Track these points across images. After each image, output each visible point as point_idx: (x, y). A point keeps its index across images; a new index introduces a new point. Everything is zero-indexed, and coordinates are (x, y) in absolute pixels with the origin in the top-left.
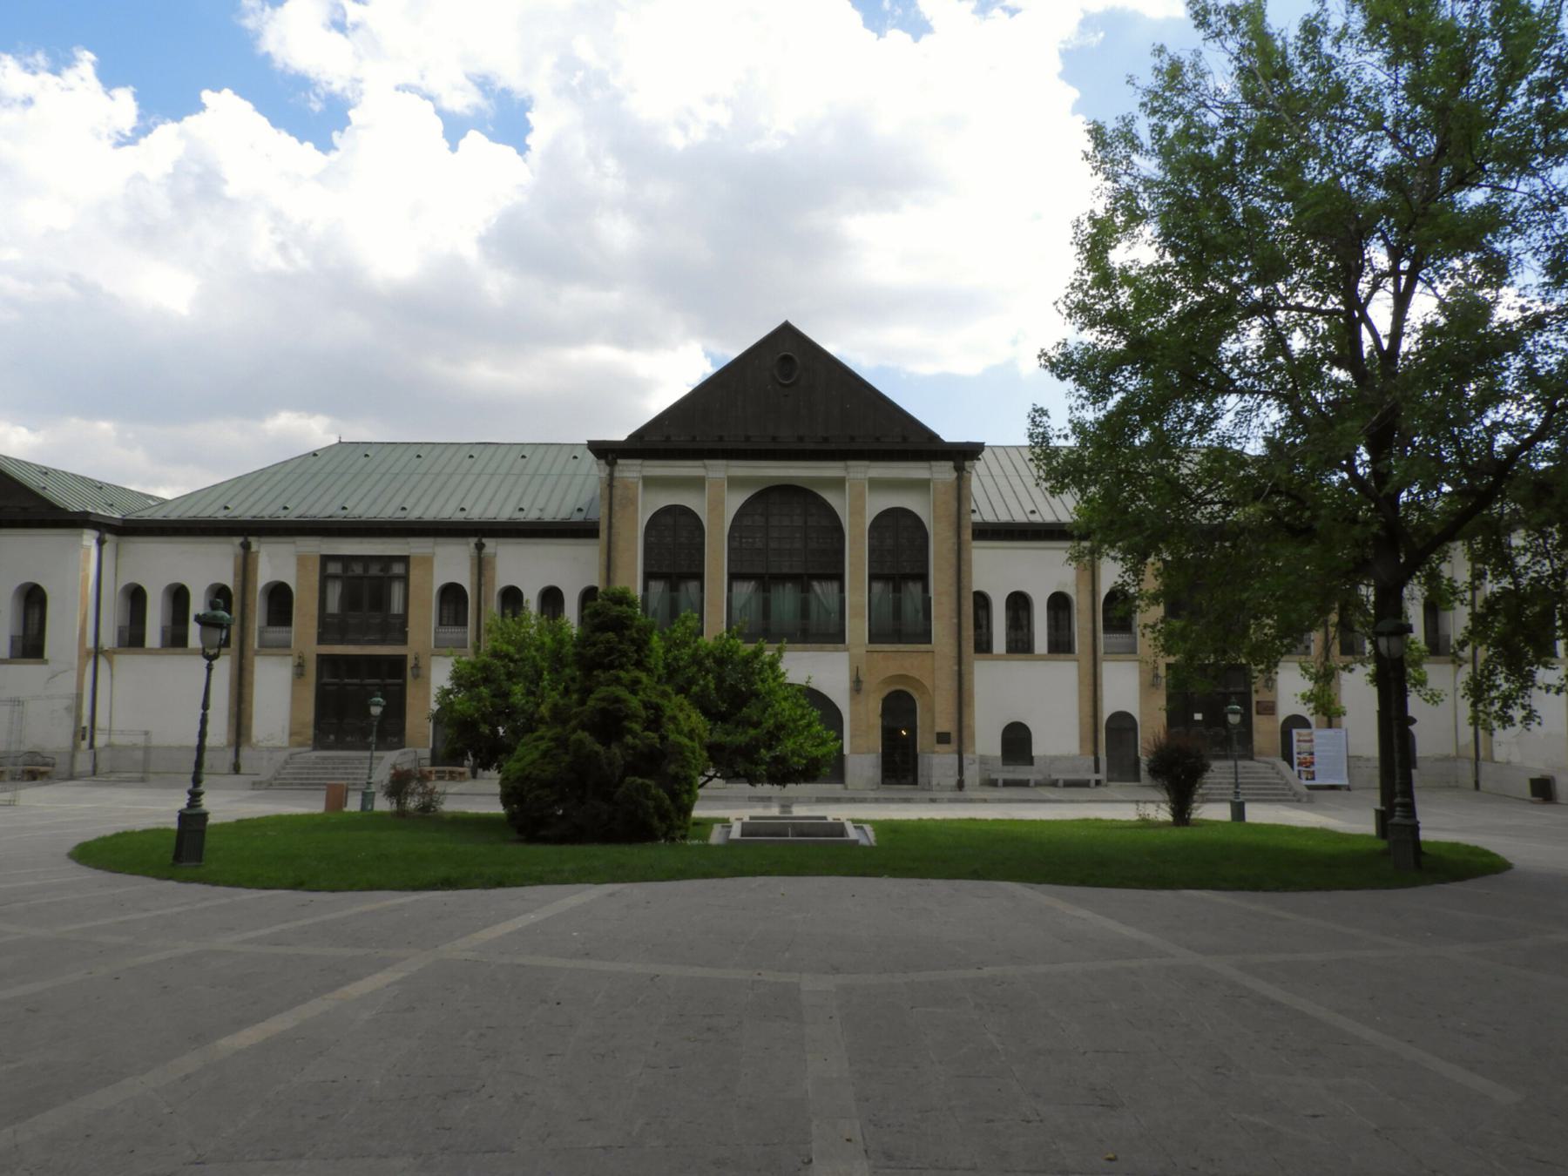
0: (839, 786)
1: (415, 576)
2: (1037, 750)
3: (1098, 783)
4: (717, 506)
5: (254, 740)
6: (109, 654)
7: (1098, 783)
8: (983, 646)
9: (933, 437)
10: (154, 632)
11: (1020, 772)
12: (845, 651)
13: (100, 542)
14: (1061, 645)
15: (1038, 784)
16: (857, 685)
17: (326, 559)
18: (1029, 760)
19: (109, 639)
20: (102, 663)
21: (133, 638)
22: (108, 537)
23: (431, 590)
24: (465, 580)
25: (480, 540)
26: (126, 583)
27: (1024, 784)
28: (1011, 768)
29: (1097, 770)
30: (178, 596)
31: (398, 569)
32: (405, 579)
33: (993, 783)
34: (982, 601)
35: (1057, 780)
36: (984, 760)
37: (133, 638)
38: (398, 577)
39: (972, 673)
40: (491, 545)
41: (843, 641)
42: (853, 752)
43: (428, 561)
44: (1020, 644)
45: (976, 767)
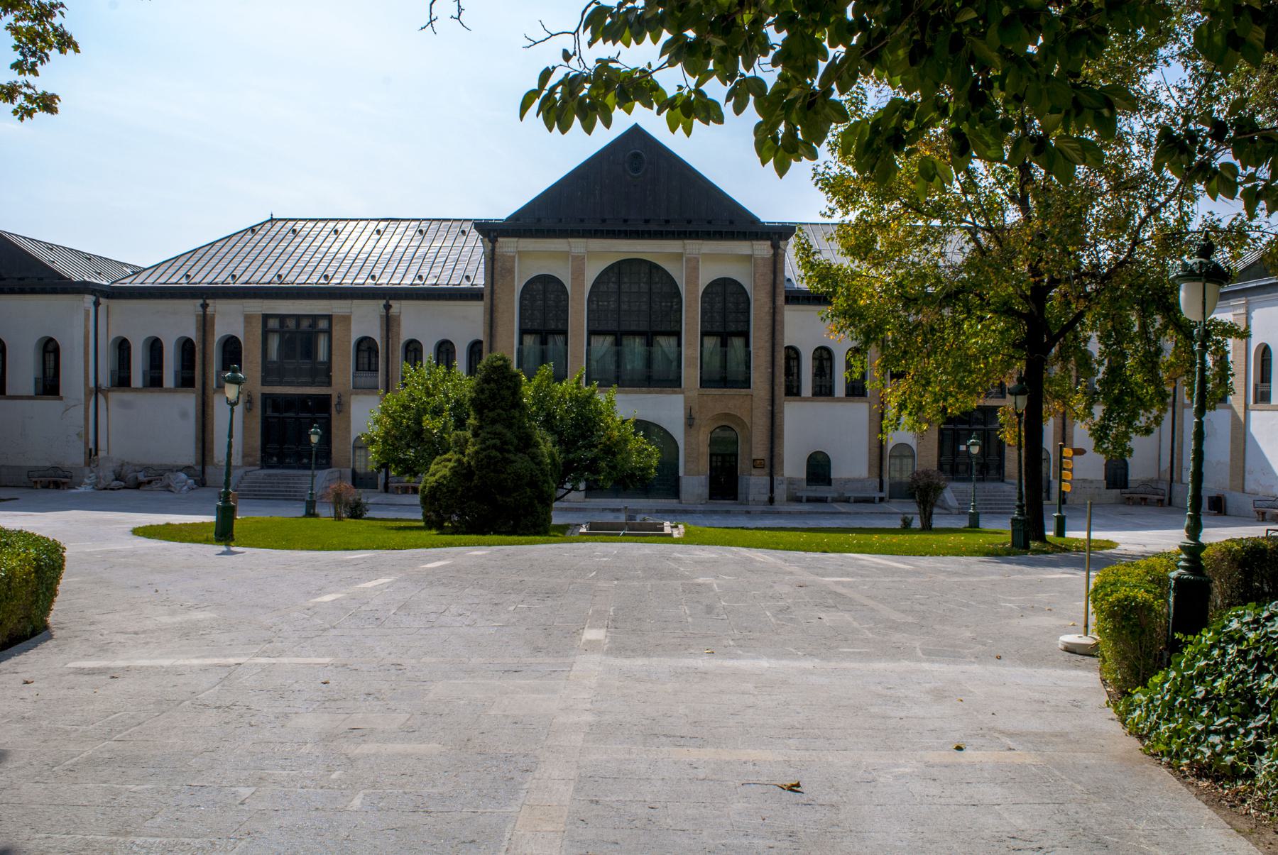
0: (675, 501)
1: (337, 330)
2: (834, 475)
3: (881, 500)
4: (578, 274)
5: (216, 460)
6: (106, 392)
7: (881, 500)
8: (793, 390)
9: (754, 220)
10: (137, 378)
11: (821, 491)
12: (680, 393)
13: (97, 304)
14: (186, 381)
15: (835, 500)
16: (690, 421)
17: (266, 317)
18: (828, 481)
19: (104, 380)
20: (100, 397)
21: (122, 380)
22: (102, 300)
23: (350, 342)
24: (376, 334)
25: (388, 302)
26: (114, 337)
27: (822, 500)
28: (814, 488)
29: (881, 490)
30: (155, 347)
31: (323, 324)
32: (329, 332)
33: (798, 500)
34: (123, 347)
35: (850, 497)
36: (791, 482)
37: (122, 380)
38: (298, 324)
39: (782, 412)
40: (396, 306)
41: (680, 386)
42: (686, 474)
43: (346, 319)
44: (154, 381)
45: (784, 486)
